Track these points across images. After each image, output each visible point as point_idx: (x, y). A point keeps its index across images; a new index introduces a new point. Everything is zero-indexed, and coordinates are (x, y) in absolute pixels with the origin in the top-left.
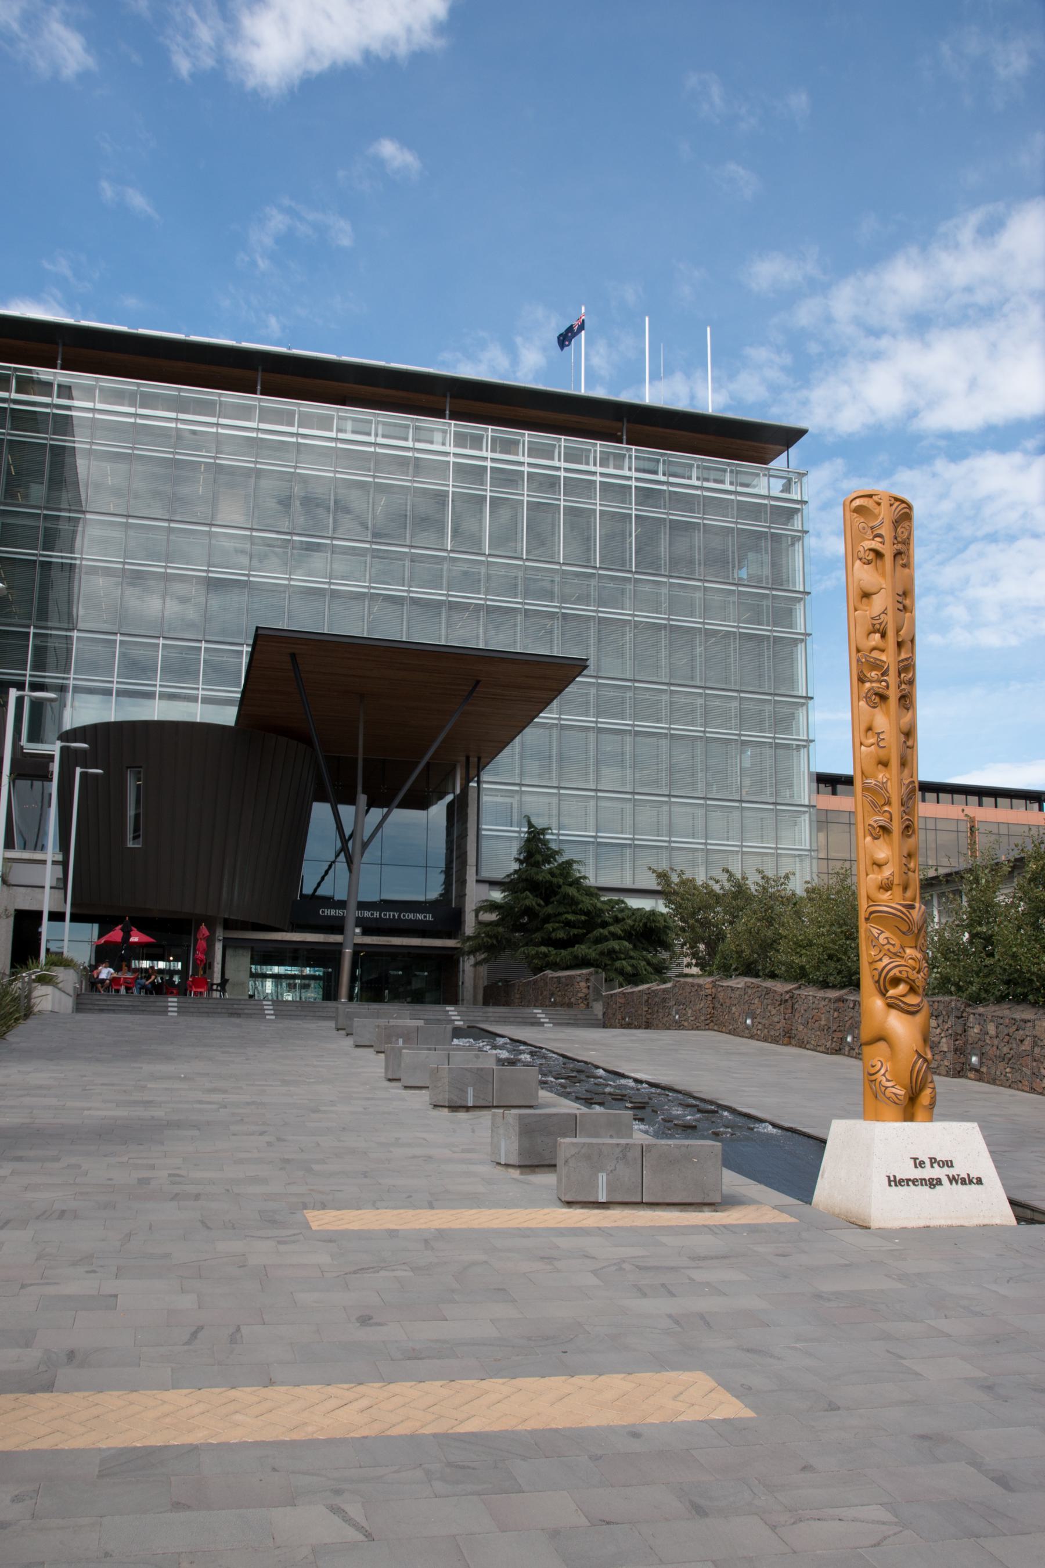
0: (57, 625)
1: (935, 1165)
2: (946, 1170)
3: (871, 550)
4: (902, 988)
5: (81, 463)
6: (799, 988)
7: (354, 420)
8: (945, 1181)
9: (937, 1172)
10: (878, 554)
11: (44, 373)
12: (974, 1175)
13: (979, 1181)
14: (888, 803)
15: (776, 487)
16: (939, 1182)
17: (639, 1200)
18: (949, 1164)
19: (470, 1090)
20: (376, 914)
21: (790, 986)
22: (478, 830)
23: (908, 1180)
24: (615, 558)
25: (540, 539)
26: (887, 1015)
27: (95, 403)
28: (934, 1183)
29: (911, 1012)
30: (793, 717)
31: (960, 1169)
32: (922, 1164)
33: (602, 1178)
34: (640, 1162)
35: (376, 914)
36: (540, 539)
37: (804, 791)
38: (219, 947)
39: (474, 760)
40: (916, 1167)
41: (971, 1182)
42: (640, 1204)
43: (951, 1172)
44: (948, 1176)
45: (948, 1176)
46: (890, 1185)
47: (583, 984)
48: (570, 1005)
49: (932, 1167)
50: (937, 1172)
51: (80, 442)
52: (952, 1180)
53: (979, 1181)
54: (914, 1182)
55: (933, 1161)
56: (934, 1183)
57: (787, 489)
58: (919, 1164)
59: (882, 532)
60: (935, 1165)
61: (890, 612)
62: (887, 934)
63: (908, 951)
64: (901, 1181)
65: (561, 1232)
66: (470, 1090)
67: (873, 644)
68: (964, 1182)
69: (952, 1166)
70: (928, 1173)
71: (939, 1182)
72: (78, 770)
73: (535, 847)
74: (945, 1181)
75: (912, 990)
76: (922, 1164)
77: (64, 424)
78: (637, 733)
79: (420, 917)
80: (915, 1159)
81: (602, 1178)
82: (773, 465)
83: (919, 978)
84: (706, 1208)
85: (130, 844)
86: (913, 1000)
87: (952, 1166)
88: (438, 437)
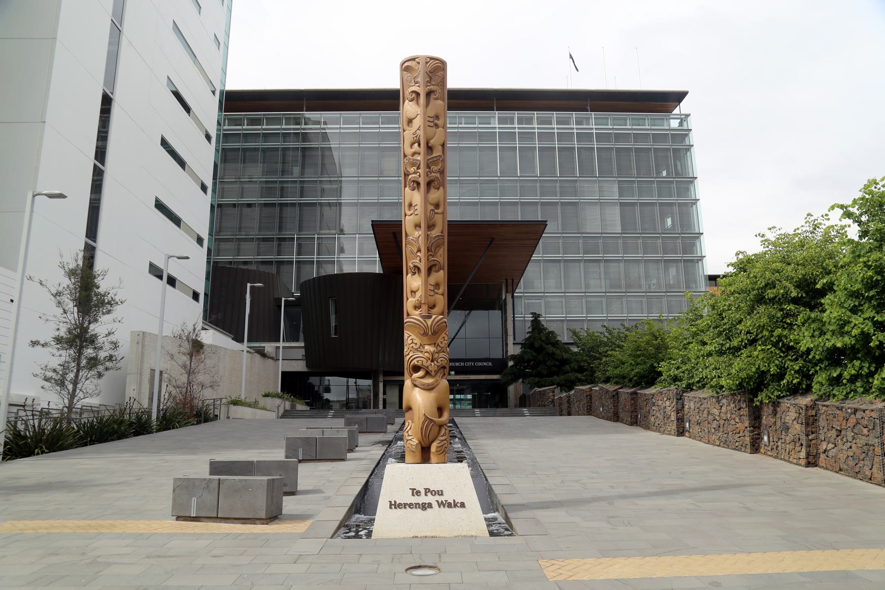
0: (328, 232)
1: (429, 494)
2: (437, 497)
3: (413, 92)
4: (421, 373)
5: (335, 154)
6: (622, 388)
7: (465, 117)
8: (435, 505)
9: (430, 499)
10: (418, 94)
11: (308, 114)
12: (459, 500)
13: (463, 505)
14: (419, 251)
15: (674, 124)
16: (430, 505)
17: (215, 515)
18: (440, 493)
19: (301, 450)
20: (462, 364)
21: (589, 386)
22: (514, 317)
23: (405, 504)
24: (567, 169)
25: (527, 163)
26: (413, 390)
27: (336, 125)
28: (425, 506)
29: (429, 388)
30: (694, 245)
31: (448, 497)
32: (418, 493)
33: (194, 500)
34: (217, 490)
35: (462, 364)
36: (527, 163)
37: (703, 286)
38: (381, 385)
39: (510, 281)
40: (413, 495)
41: (455, 506)
42: (217, 519)
43: (441, 499)
44: (437, 501)
45: (437, 501)
46: (391, 508)
47: (551, 394)
48: (545, 406)
49: (426, 495)
50: (430, 499)
51: (334, 144)
52: (441, 504)
53: (463, 505)
54: (410, 505)
55: (427, 491)
56: (425, 506)
57: (681, 124)
58: (415, 492)
59: (419, 80)
60: (429, 494)
61: (422, 128)
62: (413, 337)
63: (427, 347)
64: (400, 504)
65: (171, 536)
66: (301, 450)
67: (413, 150)
68: (450, 505)
69: (442, 494)
70: (422, 499)
71: (430, 505)
72: (249, 285)
73: (536, 322)
74: (435, 505)
75: (428, 374)
76: (418, 493)
77: (325, 137)
78: (606, 261)
79: (485, 364)
80: (413, 490)
81: (194, 500)
82: (674, 112)
83: (433, 367)
84: (258, 522)
85: (333, 336)
86: (429, 381)
87: (442, 494)
88: (492, 121)
